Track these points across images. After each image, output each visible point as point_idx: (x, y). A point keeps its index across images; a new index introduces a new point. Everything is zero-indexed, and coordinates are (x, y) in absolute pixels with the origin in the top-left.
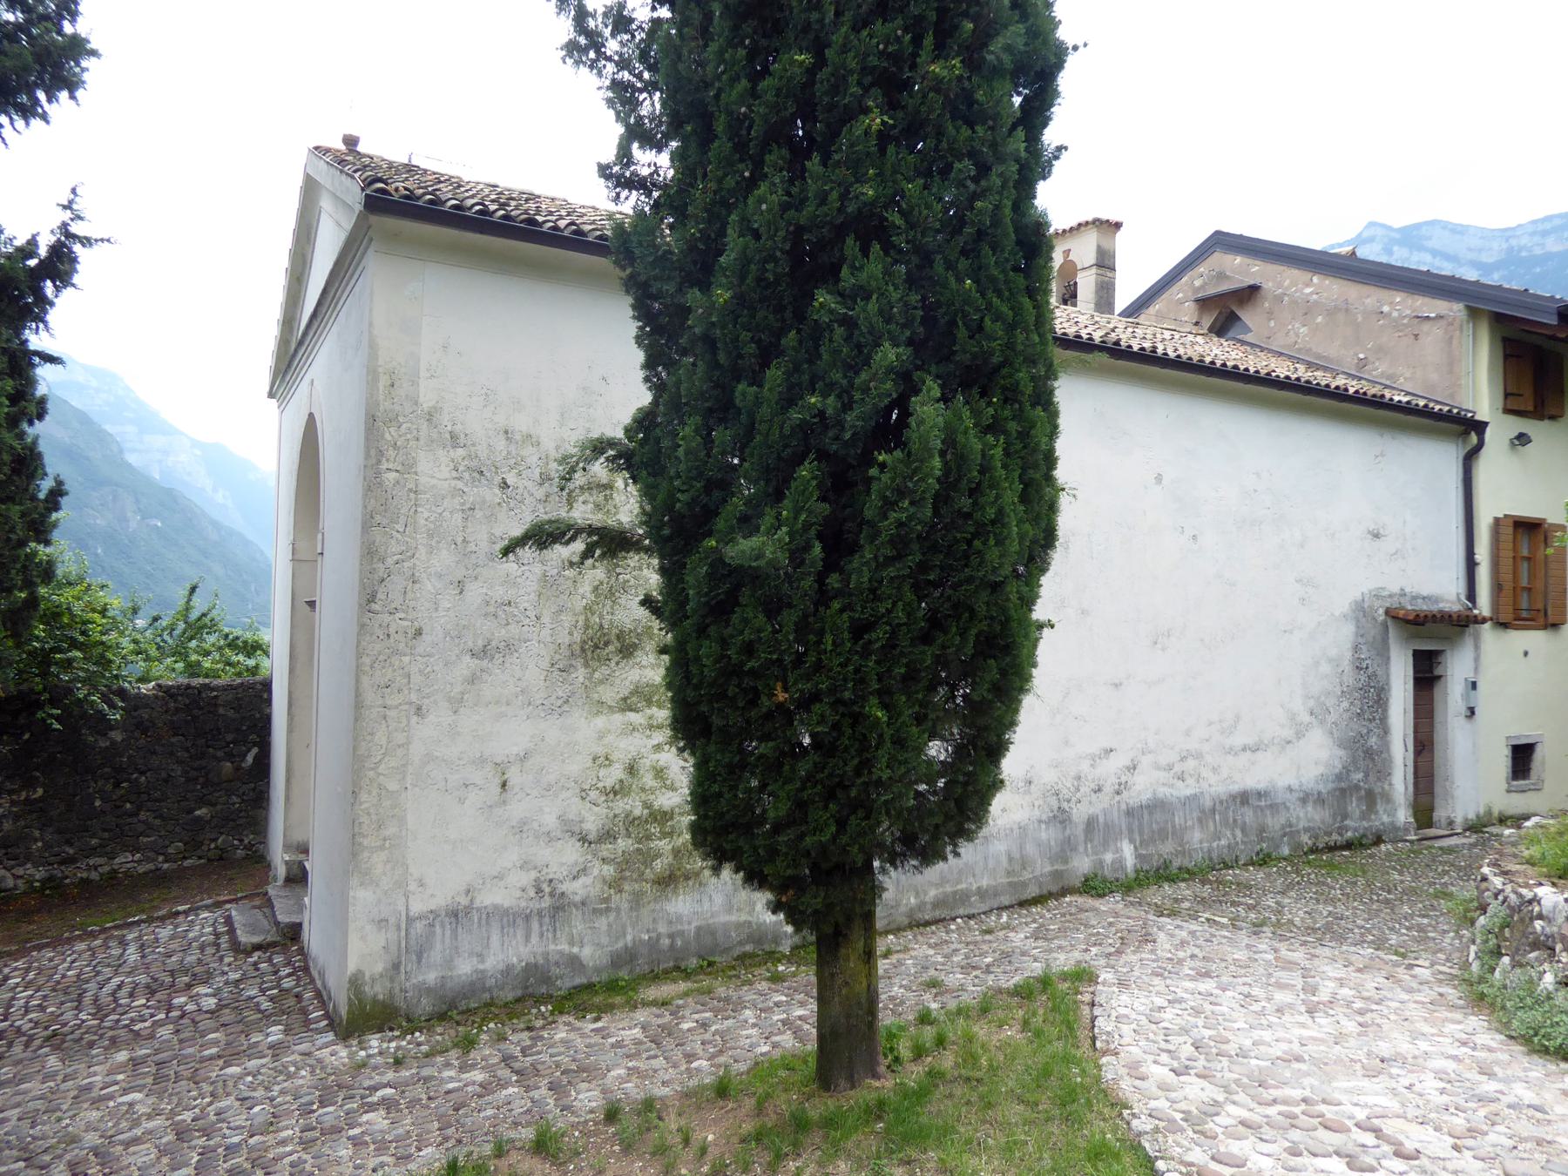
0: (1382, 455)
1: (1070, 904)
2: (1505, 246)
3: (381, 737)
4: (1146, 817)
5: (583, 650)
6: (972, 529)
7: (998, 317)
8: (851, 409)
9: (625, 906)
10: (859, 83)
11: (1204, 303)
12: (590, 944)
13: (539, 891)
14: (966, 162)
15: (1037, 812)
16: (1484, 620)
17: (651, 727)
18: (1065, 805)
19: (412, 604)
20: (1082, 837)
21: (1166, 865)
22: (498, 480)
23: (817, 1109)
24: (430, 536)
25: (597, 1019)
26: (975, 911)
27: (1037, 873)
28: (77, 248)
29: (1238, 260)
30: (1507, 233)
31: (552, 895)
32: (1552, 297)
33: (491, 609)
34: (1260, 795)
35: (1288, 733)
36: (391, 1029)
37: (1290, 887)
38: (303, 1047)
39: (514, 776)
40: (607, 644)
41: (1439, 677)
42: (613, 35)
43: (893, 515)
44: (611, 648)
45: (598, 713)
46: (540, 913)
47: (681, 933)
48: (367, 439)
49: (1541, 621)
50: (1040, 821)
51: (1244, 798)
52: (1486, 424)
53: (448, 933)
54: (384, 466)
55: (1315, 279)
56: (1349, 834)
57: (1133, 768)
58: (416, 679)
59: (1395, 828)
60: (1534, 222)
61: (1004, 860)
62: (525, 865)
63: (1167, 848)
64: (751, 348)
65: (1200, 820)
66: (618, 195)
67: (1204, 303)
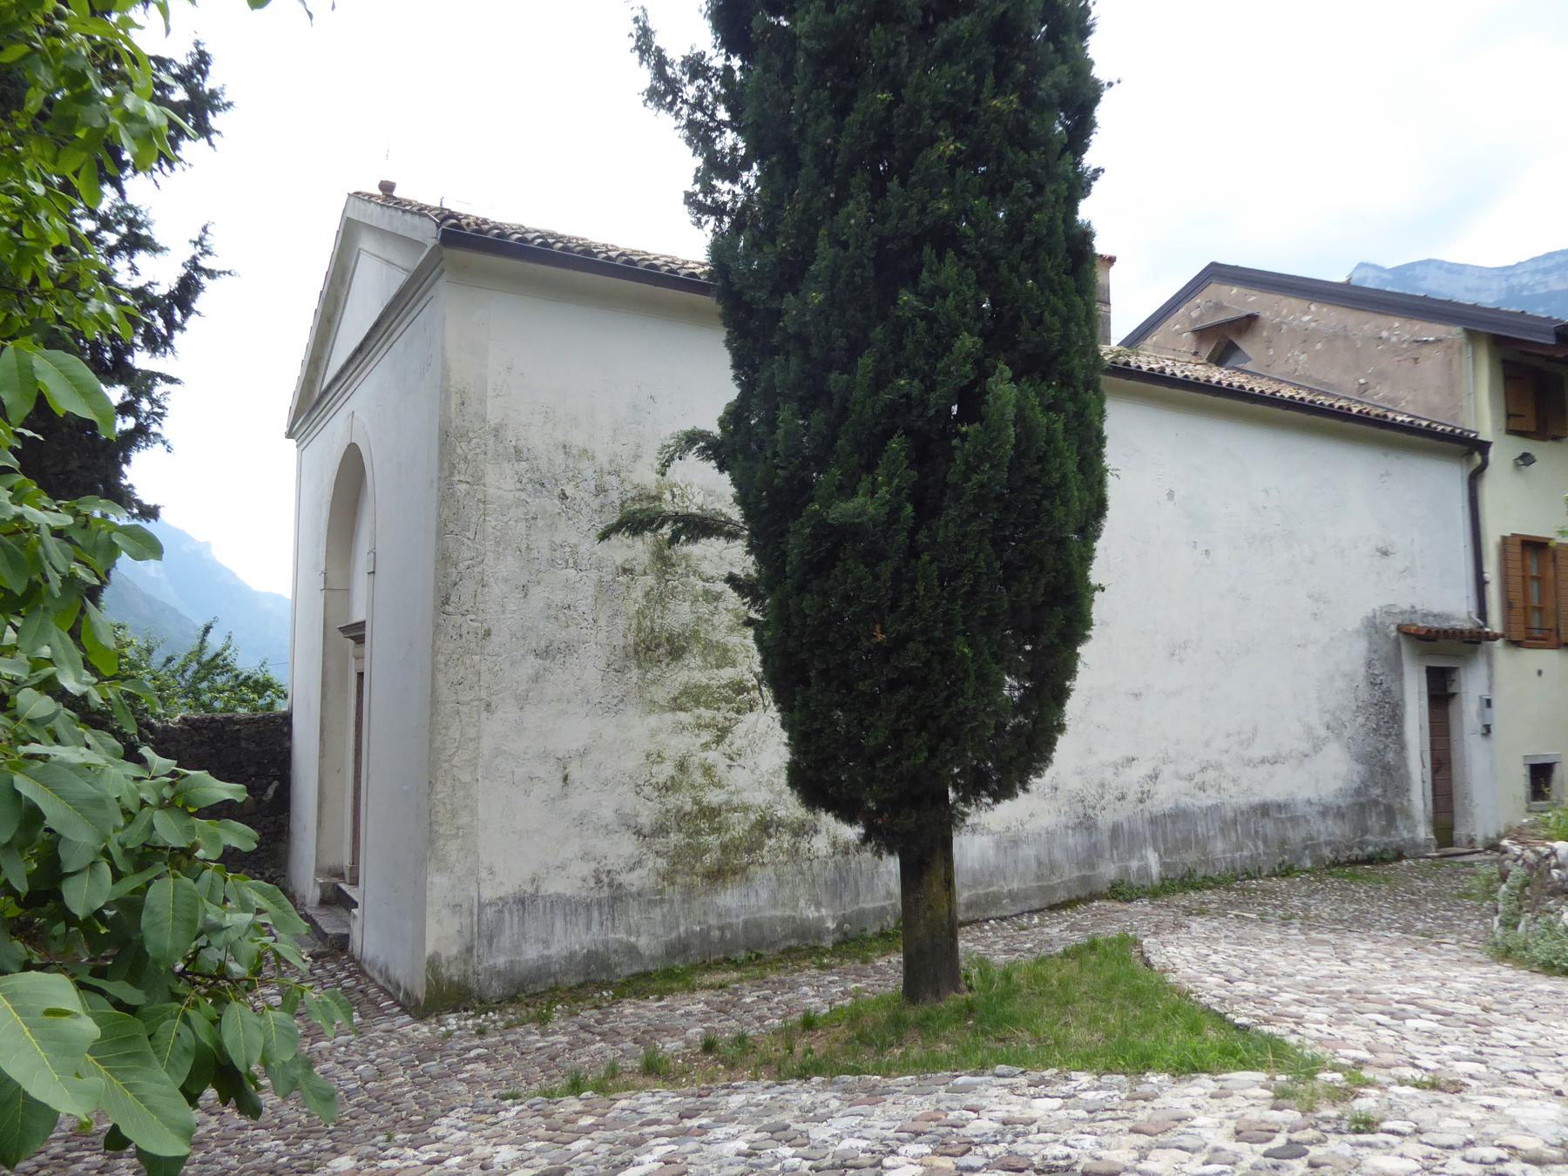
0: (1388, 474)
1: (1098, 908)
2: (1504, 285)
3: (454, 732)
4: (1169, 826)
5: (636, 652)
6: (1040, 492)
7: (1055, 312)
8: (934, 390)
9: (678, 897)
10: (932, 117)
11: (1202, 334)
12: (647, 936)
13: (598, 881)
14: (1024, 181)
15: (1063, 818)
16: (1495, 637)
17: (699, 726)
18: (1090, 812)
19: (482, 606)
20: (1107, 844)
21: (1191, 873)
22: (557, 491)
23: (912, 1014)
24: (498, 543)
25: (660, 999)
26: (1006, 914)
27: (1066, 878)
28: (204, 279)
29: (1235, 290)
30: (1506, 272)
31: (610, 885)
32: (1549, 319)
33: (553, 612)
34: (1280, 807)
35: (1305, 747)
36: (466, 1010)
37: (1316, 891)
38: (384, 1026)
40: (658, 646)
41: (1454, 695)
42: (691, 81)
43: (975, 478)
44: (662, 650)
45: (651, 712)
46: (600, 903)
47: (730, 926)
48: (441, 453)
49: (1554, 639)
50: (1067, 827)
51: (1264, 810)
52: (1488, 444)
53: (516, 919)
54: (456, 478)
55: (1313, 308)
56: (1370, 849)
57: (1154, 777)
58: (486, 678)
59: (1414, 844)
60: (1534, 260)
61: (1034, 865)
62: (585, 856)
63: (1191, 857)
64: (843, 342)
65: (1222, 830)
66: (699, 220)
67: (1202, 334)
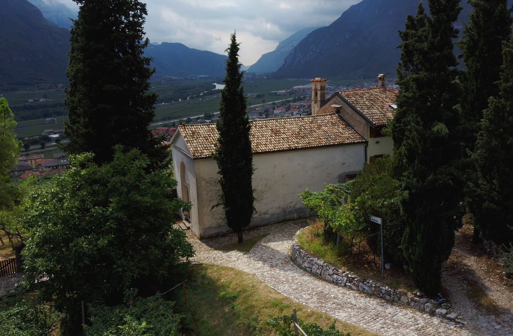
39: (214, 213)
57: (296, 204)
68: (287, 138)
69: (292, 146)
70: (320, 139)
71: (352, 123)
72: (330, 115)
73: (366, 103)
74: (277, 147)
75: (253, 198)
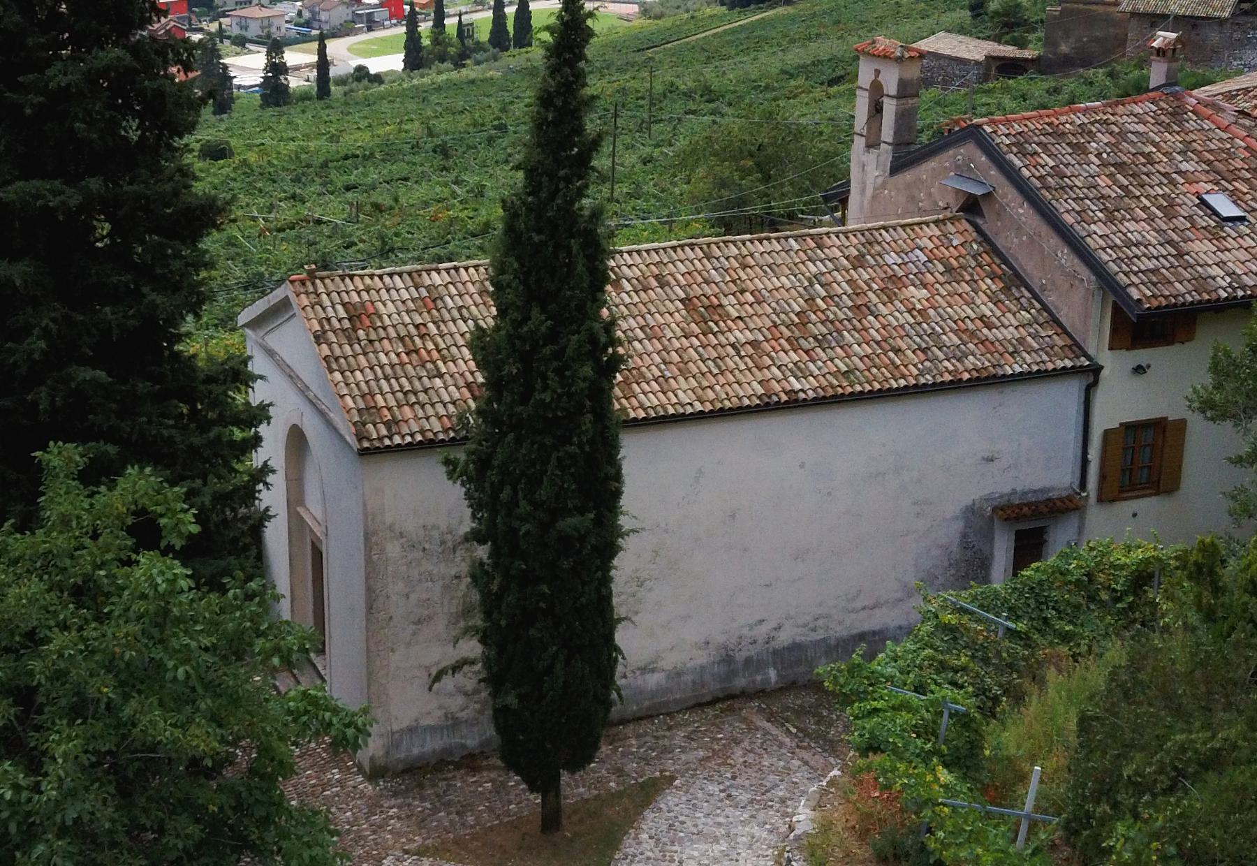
57: (779, 628)
68: (754, 344)
69: (778, 388)
70: (897, 351)
71: (1036, 277)
72: (936, 222)
73: (1102, 181)
74: (710, 394)
75: (618, 649)
